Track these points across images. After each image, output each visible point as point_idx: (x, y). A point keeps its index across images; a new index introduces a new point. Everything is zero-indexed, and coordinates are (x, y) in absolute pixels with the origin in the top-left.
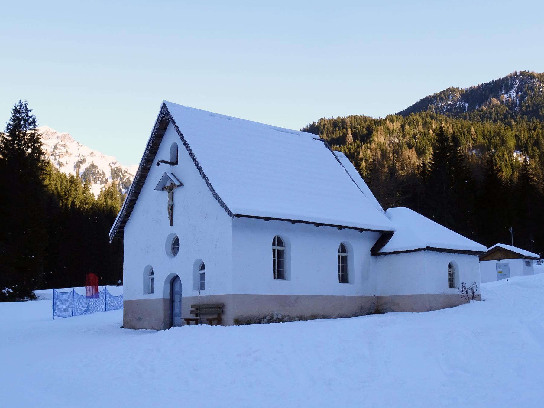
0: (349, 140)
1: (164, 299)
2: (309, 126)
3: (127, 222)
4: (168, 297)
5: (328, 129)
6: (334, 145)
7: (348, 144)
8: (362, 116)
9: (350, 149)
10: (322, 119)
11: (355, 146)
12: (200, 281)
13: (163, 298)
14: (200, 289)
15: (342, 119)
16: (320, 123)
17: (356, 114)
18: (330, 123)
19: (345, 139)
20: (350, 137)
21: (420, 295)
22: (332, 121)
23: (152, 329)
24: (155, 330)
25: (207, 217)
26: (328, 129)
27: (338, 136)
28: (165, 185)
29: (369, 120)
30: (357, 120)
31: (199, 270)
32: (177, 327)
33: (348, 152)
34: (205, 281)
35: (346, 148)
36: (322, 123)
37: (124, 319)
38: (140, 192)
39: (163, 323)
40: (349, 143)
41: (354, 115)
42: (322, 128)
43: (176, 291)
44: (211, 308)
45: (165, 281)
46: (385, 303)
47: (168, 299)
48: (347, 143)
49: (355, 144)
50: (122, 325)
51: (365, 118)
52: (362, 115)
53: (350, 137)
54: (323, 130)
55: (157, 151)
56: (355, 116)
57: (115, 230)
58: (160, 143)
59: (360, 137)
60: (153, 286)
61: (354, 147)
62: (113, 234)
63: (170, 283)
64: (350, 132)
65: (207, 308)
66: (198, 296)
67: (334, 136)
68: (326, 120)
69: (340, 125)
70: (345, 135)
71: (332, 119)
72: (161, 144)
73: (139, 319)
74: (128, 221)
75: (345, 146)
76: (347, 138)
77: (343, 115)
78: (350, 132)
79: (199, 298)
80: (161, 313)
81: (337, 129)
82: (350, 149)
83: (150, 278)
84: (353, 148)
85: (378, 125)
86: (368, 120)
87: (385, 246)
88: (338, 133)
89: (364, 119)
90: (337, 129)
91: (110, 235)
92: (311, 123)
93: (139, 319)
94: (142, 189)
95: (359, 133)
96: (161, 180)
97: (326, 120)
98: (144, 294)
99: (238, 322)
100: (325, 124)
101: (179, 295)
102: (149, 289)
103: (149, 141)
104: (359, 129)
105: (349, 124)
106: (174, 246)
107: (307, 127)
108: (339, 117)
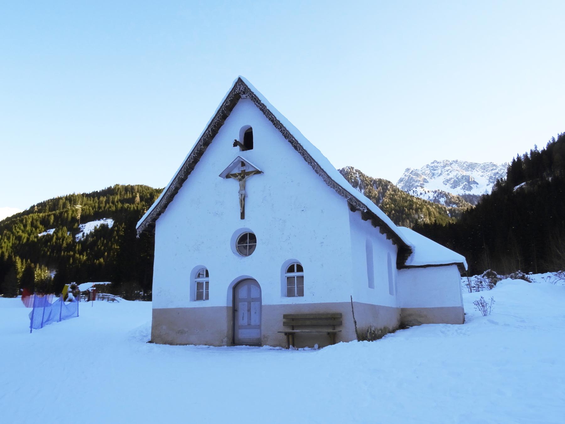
0: (137, 201)
1: (227, 307)
2: (106, 188)
3: (162, 214)
4: (231, 305)
5: (121, 192)
6: (126, 203)
7: (136, 204)
8: (145, 186)
9: (137, 207)
10: (117, 185)
11: (141, 205)
12: (196, 290)
13: (226, 305)
14: (286, 295)
15: (131, 186)
16: (116, 187)
17: (142, 184)
18: (123, 188)
19: (134, 200)
20: (138, 199)
21: (453, 307)
22: (124, 187)
23: (206, 345)
24: (211, 347)
25: (304, 210)
26: (121, 192)
27: (128, 197)
28: (231, 172)
29: (151, 189)
30: (142, 188)
31: (196, 278)
32: (350, 342)
33: (136, 209)
34: (303, 285)
35: (134, 205)
36: (117, 188)
37: (152, 333)
38: (186, 180)
39: (226, 337)
40: (137, 203)
41: (140, 184)
42: (117, 190)
43: (239, 298)
44: (320, 319)
45: (229, 287)
46: (410, 315)
47: (230, 307)
48: (136, 203)
49: (142, 204)
50: (149, 338)
51: (148, 187)
52: (146, 185)
53: (138, 199)
54: (117, 192)
55: (216, 134)
56: (141, 185)
57: (147, 222)
58: (222, 125)
59: (145, 200)
60: (303, 286)
61: (140, 205)
62: (143, 227)
63: (233, 288)
64: (138, 195)
65: (313, 319)
66: (351, 301)
67: (125, 197)
68: (120, 186)
69: (129, 190)
70: (134, 197)
71: (125, 186)
72: (222, 126)
73: (181, 332)
74: (163, 213)
75: (134, 204)
76: (136, 199)
77: (132, 184)
78: (138, 195)
79: (352, 304)
80: (224, 324)
81: (128, 192)
82: (137, 207)
83: (196, 281)
84: (140, 207)
85: (159, 193)
86: (150, 189)
87: (407, 259)
88: (129, 195)
89: (148, 188)
90: (128, 192)
91: (138, 229)
92: (109, 186)
93: (181, 332)
94: (189, 176)
95: (145, 197)
96: (232, 165)
97: (120, 186)
98: (190, 301)
99: (362, 337)
100: (119, 188)
101: (246, 303)
102: (195, 293)
103: (213, 120)
104: (145, 194)
105: (136, 190)
106: (238, 244)
107: (105, 189)
108: (129, 185)
